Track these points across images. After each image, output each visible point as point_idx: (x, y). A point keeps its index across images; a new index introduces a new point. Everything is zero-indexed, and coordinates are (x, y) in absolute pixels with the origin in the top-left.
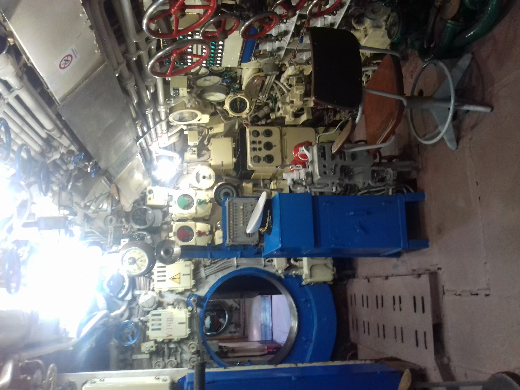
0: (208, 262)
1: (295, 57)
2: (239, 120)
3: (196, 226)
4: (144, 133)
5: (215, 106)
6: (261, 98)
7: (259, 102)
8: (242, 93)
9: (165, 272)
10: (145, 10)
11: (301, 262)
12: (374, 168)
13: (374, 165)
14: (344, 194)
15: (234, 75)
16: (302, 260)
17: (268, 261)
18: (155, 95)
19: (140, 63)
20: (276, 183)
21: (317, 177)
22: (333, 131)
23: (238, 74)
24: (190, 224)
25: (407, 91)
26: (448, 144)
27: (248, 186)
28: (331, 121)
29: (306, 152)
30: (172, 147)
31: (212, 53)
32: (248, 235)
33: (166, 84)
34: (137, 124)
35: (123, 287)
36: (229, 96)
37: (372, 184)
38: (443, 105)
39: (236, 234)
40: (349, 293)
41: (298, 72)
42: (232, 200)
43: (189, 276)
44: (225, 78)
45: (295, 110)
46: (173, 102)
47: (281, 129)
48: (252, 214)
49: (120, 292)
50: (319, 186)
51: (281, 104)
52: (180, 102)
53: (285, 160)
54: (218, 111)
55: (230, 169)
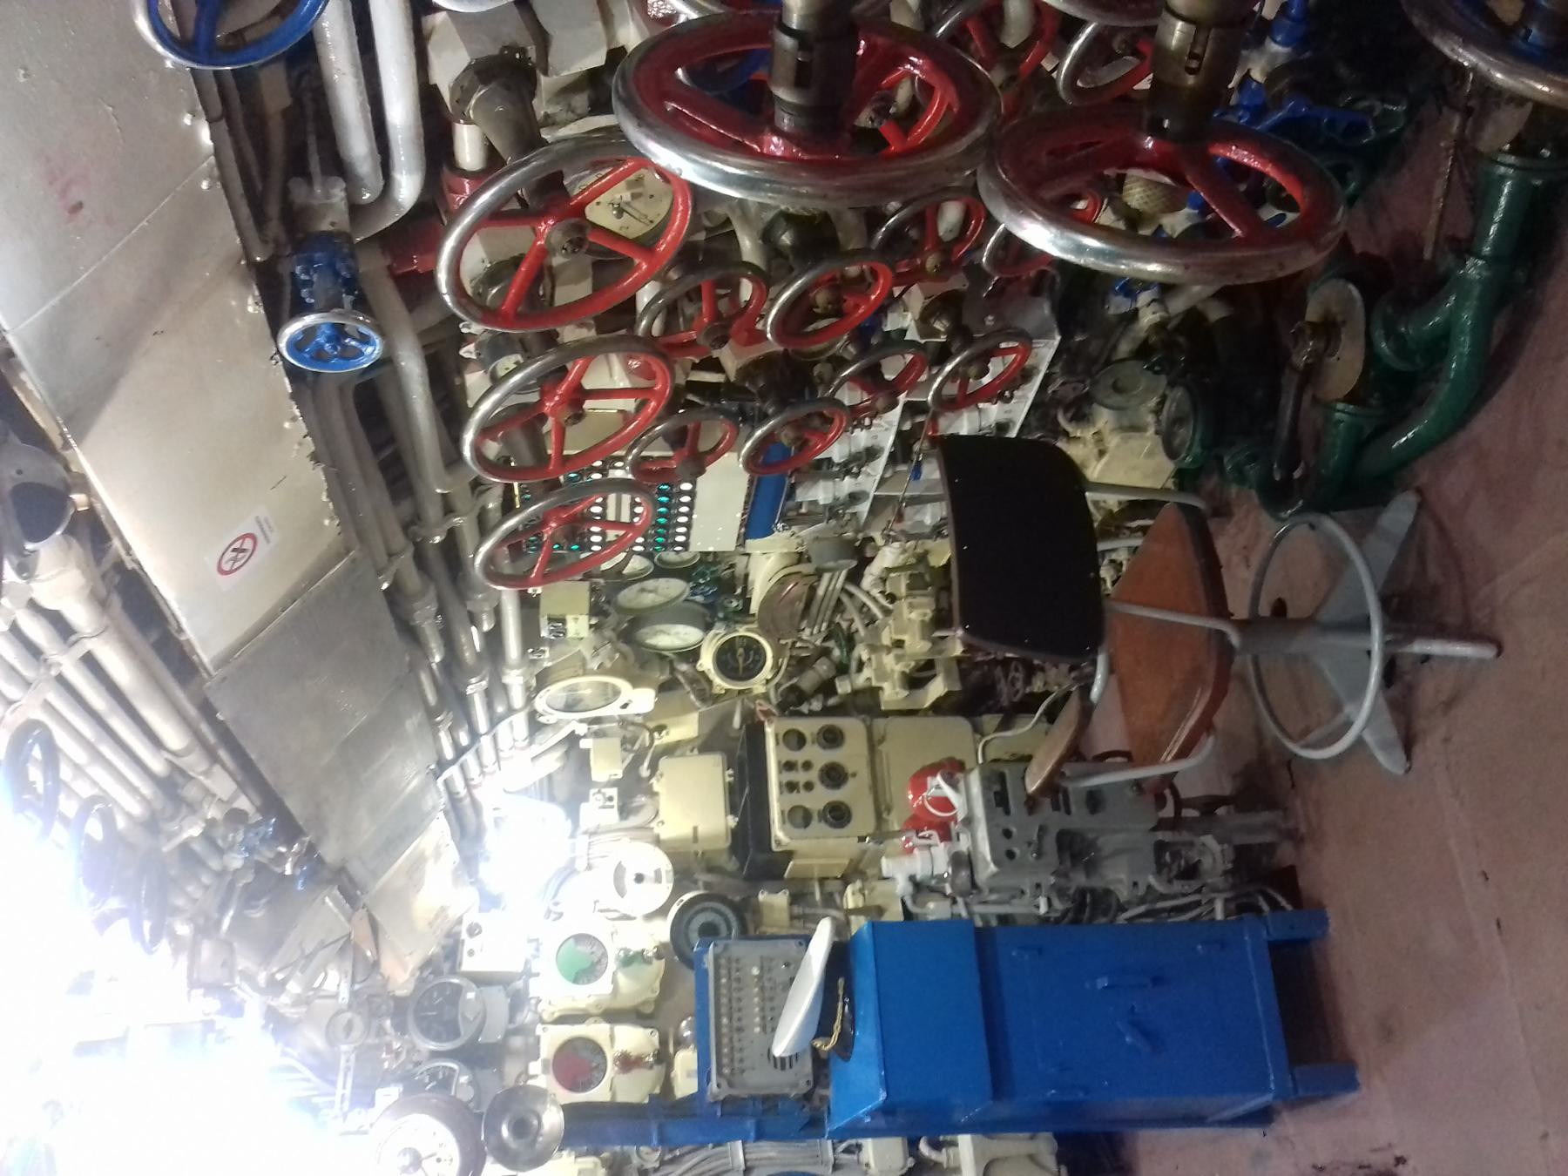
1: (900, 517)
3: (612, 1038)
4: (460, 751)
5: (671, 662)
6: (806, 635)
10: (470, 404)
11: (951, 1151)
12: (1161, 836)
13: (1161, 825)
14: (1076, 921)
16: (954, 1144)
17: (844, 1152)
18: (494, 639)
19: (452, 551)
20: (861, 891)
21: (987, 868)
23: (739, 570)
24: (596, 1031)
25: (1239, 606)
26: (1381, 757)
27: (775, 901)
28: (1019, 696)
29: (948, 791)
30: (547, 788)
33: (529, 605)
36: (712, 633)
37: (1160, 887)
38: (1352, 642)
39: (741, 1060)
41: (913, 560)
42: (726, 948)
44: (701, 581)
46: (547, 655)
48: (791, 993)
50: (994, 897)
53: (885, 815)
54: (680, 677)
55: (719, 852)
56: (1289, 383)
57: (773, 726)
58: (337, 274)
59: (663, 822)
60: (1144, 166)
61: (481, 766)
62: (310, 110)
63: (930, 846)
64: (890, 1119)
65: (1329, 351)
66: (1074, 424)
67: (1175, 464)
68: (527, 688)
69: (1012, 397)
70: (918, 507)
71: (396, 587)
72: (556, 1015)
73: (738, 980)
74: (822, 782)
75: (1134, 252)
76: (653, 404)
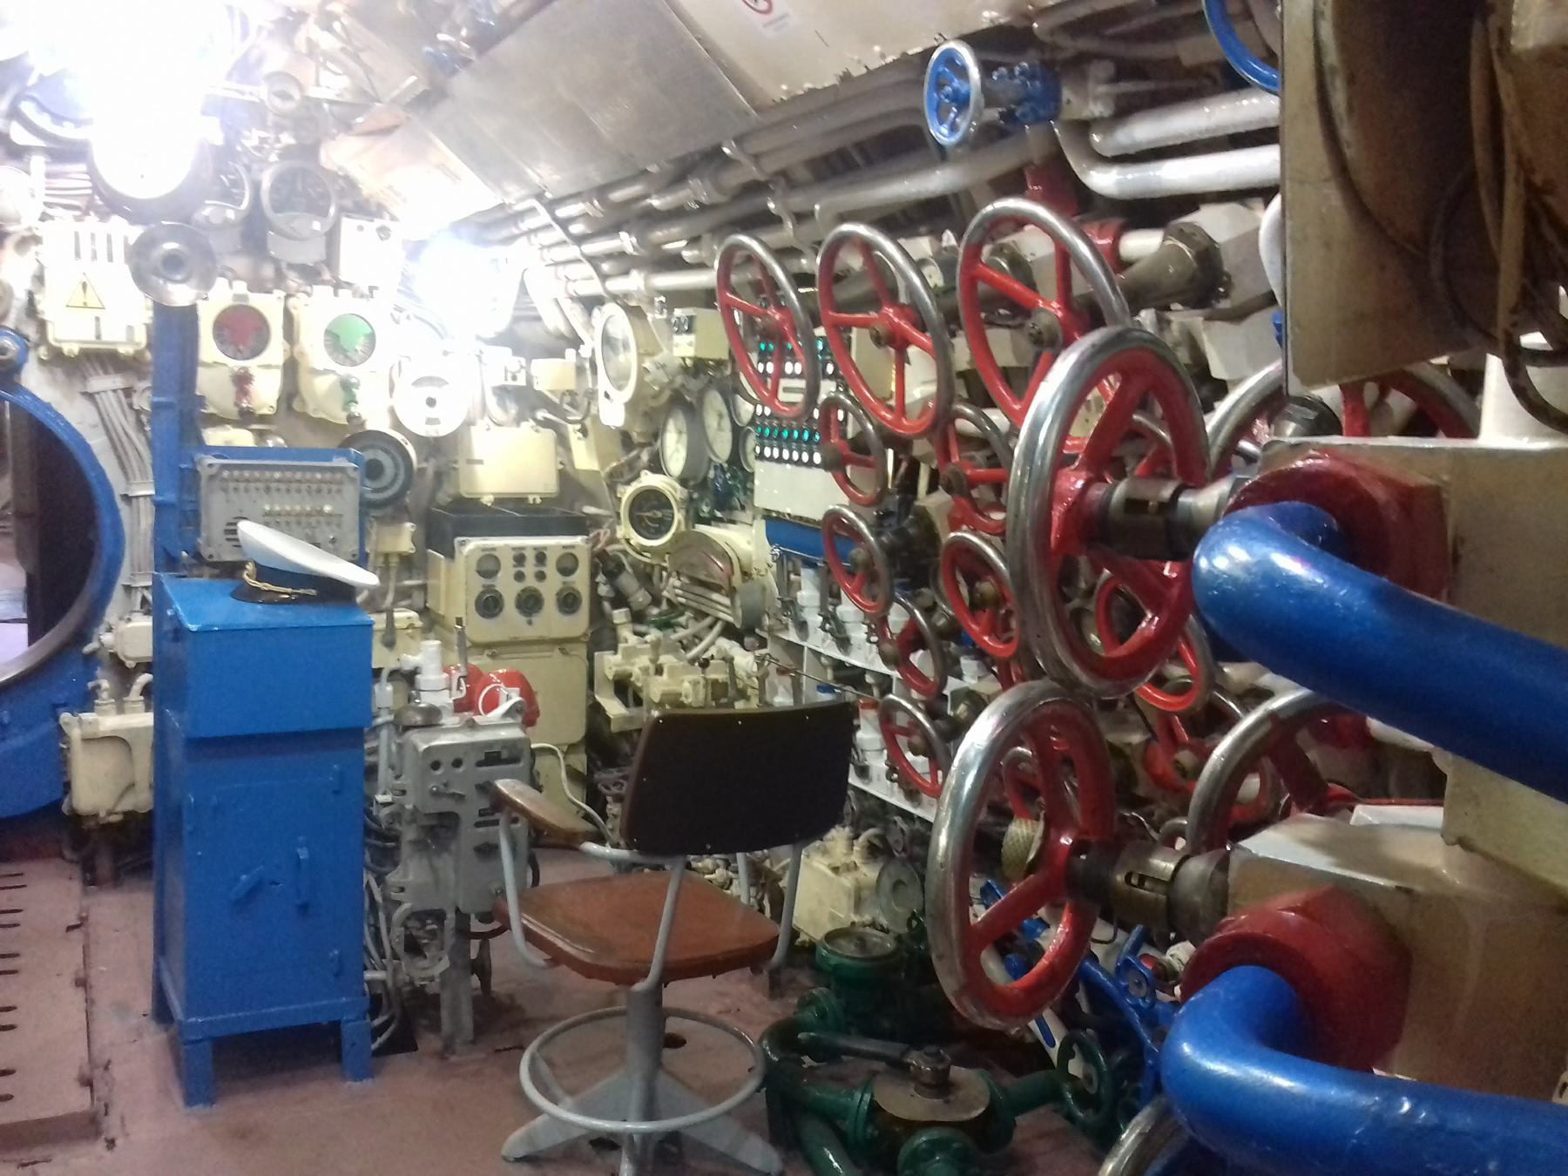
0: (143, 402)
1: (782, 671)
2: (611, 517)
3: (268, 367)
4: (564, 224)
5: (650, 444)
6: (674, 581)
7: (661, 575)
8: (687, 526)
9: (110, 258)
10: (902, 241)
11: (141, 706)
12: (451, 915)
13: (462, 917)
14: (368, 832)
15: (736, 502)
16: (147, 710)
18: (675, 263)
19: (760, 221)
20: (411, 626)
21: (422, 741)
22: (574, 795)
23: (739, 515)
24: (276, 351)
25: (678, 994)
26: (519, 1133)
27: (404, 539)
28: (604, 790)
29: (504, 707)
30: (526, 314)
31: (791, 434)
32: (232, 527)
33: (706, 298)
34: (592, 203)
35: (58, 119)
36: (678, 486)
37: (398, 914)
38: (635, 1097)
39: (236, 489)
40: (32, 869)
41: (740, 686)
42: (353, 480)
43: (93, 338)
44: (728, 475)
45: (638, 680)
46: (658, 316)
47: (583, 639)
48: (304, 543)
49: (42, 108)
50: (394, 748)
51: (654, 639)
52: (658, 338)
53: (487, 652)
54: (634, 453)
55: (458, 486)
56: (892, 1049)
57: (582, 544)
58: (1019, 103)
59: (488, 429)
60: (1046, 836)
61: (550, 246)
62: (1180, 84)
63: (450, 689)
64: (171, 635)
65: (923, 1088)
66: (866, 844)
67: (821, 941)
68: (626, 295)
69: (892, 780)
70: (791, 691)
71: (727, 161)
72: (293, 311)
73: (319, 491)
74: (523, 591)
75: (959, 821)
76: (889, 416)
